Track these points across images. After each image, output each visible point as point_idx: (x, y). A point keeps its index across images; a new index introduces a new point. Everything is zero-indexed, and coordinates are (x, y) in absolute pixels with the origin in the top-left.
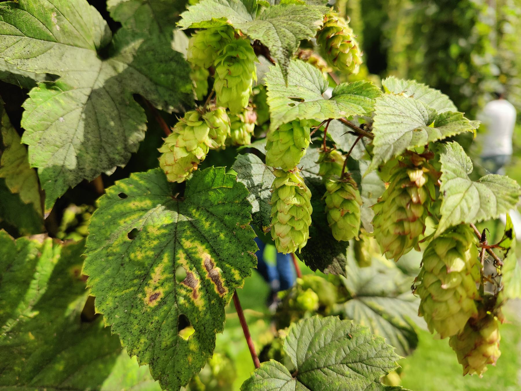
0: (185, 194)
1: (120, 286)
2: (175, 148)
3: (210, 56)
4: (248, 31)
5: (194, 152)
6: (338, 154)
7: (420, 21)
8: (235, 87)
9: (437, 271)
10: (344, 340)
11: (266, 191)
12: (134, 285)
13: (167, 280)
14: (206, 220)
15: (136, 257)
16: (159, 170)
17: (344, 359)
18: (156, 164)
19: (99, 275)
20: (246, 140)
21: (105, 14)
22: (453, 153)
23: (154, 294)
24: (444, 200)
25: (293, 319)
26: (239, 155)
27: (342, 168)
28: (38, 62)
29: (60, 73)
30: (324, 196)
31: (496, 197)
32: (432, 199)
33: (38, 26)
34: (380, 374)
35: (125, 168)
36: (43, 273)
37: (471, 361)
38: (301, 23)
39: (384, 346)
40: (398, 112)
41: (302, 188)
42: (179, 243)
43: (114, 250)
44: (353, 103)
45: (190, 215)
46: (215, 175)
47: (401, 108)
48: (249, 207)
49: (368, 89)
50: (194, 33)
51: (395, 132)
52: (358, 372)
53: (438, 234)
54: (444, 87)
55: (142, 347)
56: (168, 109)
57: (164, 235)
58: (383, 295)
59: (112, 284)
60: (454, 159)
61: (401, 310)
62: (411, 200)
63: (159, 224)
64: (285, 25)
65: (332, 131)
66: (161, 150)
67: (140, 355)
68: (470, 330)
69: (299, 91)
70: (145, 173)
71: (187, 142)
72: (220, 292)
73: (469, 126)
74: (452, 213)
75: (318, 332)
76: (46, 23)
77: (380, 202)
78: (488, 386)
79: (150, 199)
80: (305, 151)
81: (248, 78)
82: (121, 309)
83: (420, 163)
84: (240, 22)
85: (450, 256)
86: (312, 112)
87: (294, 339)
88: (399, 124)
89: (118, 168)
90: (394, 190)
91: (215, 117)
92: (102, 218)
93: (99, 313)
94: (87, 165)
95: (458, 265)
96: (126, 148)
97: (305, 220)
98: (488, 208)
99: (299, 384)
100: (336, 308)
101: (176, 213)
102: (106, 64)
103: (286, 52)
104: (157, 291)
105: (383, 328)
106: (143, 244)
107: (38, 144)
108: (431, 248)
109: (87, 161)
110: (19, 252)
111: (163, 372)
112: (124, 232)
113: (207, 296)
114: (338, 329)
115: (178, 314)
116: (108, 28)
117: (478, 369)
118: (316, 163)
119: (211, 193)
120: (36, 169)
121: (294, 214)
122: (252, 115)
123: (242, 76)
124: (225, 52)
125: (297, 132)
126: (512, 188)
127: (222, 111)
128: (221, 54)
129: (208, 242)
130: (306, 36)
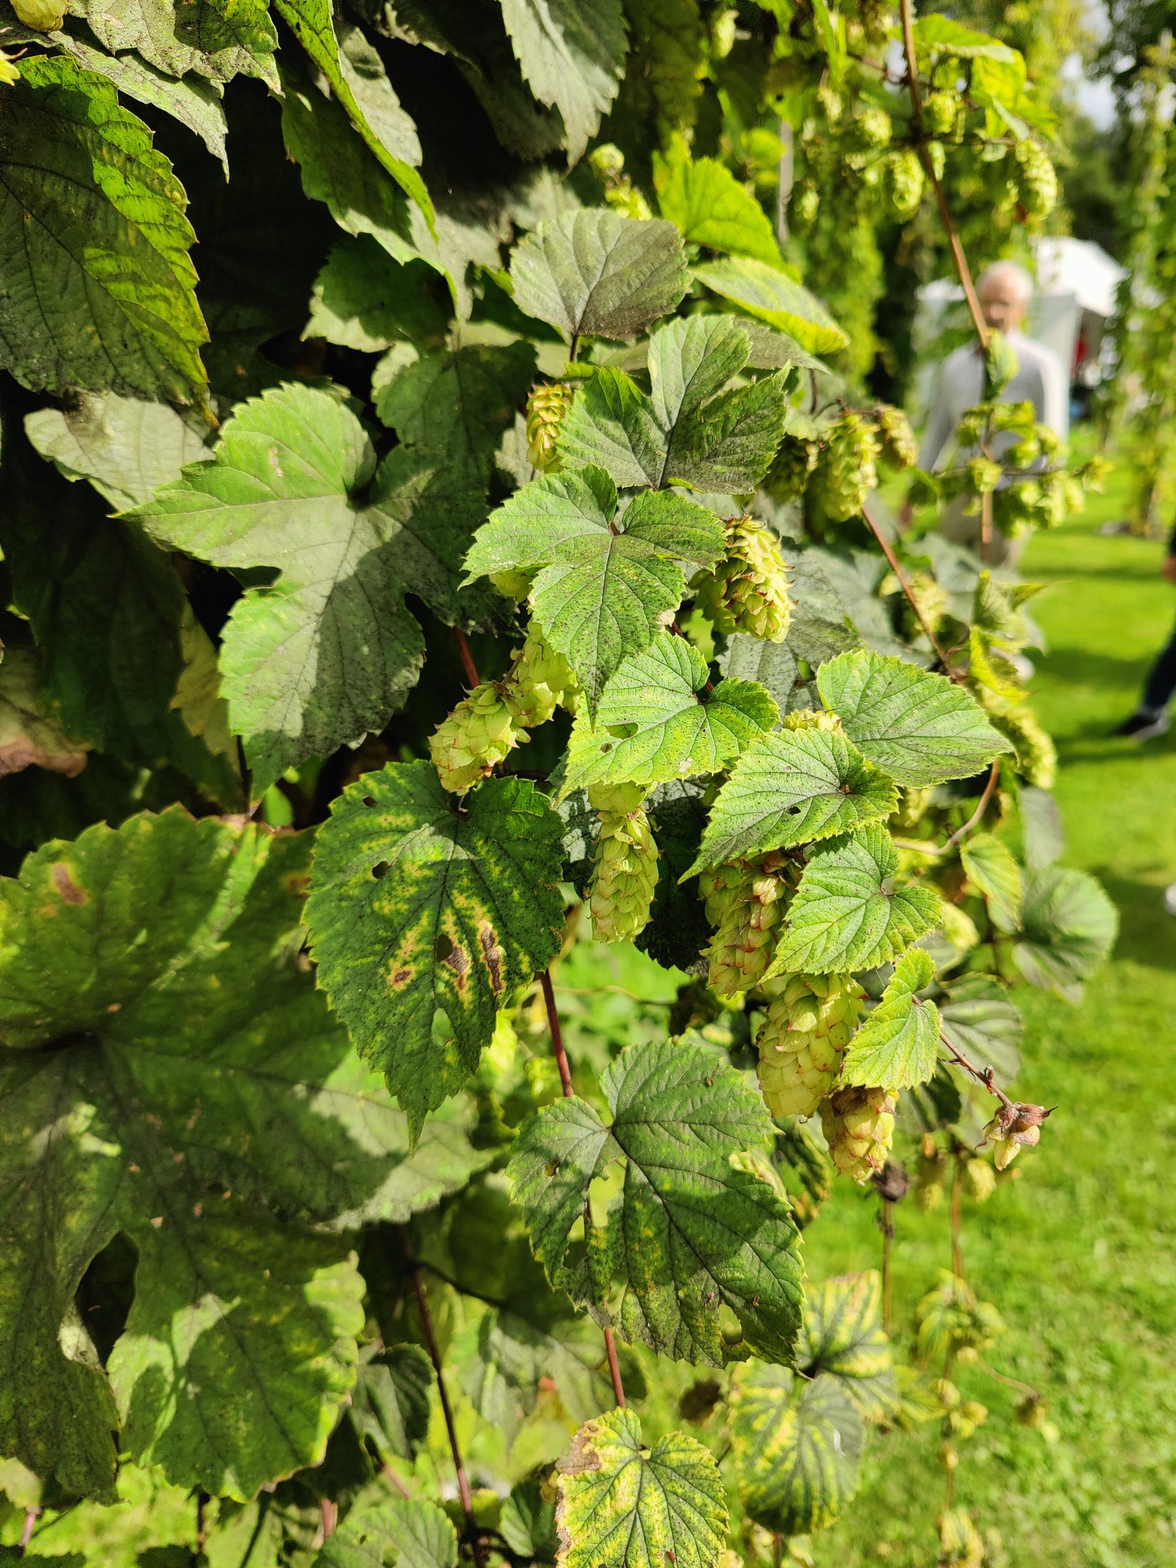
1: (354, 951)
14: (496, 864)
21: (367, 413)
25: (694, 1021)
36: (240, 879)
45: (473, 849)
46: (517, 790)
55: (376, 1047)
56: (466, 626)
57: (427, 880)
59: (343, 946)
63: (421, 859)
71: (473, 741)
79: (413, 813)
85: (801, 1005)
87: (621, 1070)
92: (336, 836)
96: (384, 699)
99: (613, 1139)
101: (452, 843)
102: (362, 516)
104: (407, 968)
110: (203, 842)
111: (404, 1086)
116: (371, 447)
119: (510, 818)
120: (239, 738)
121: (621, 887)
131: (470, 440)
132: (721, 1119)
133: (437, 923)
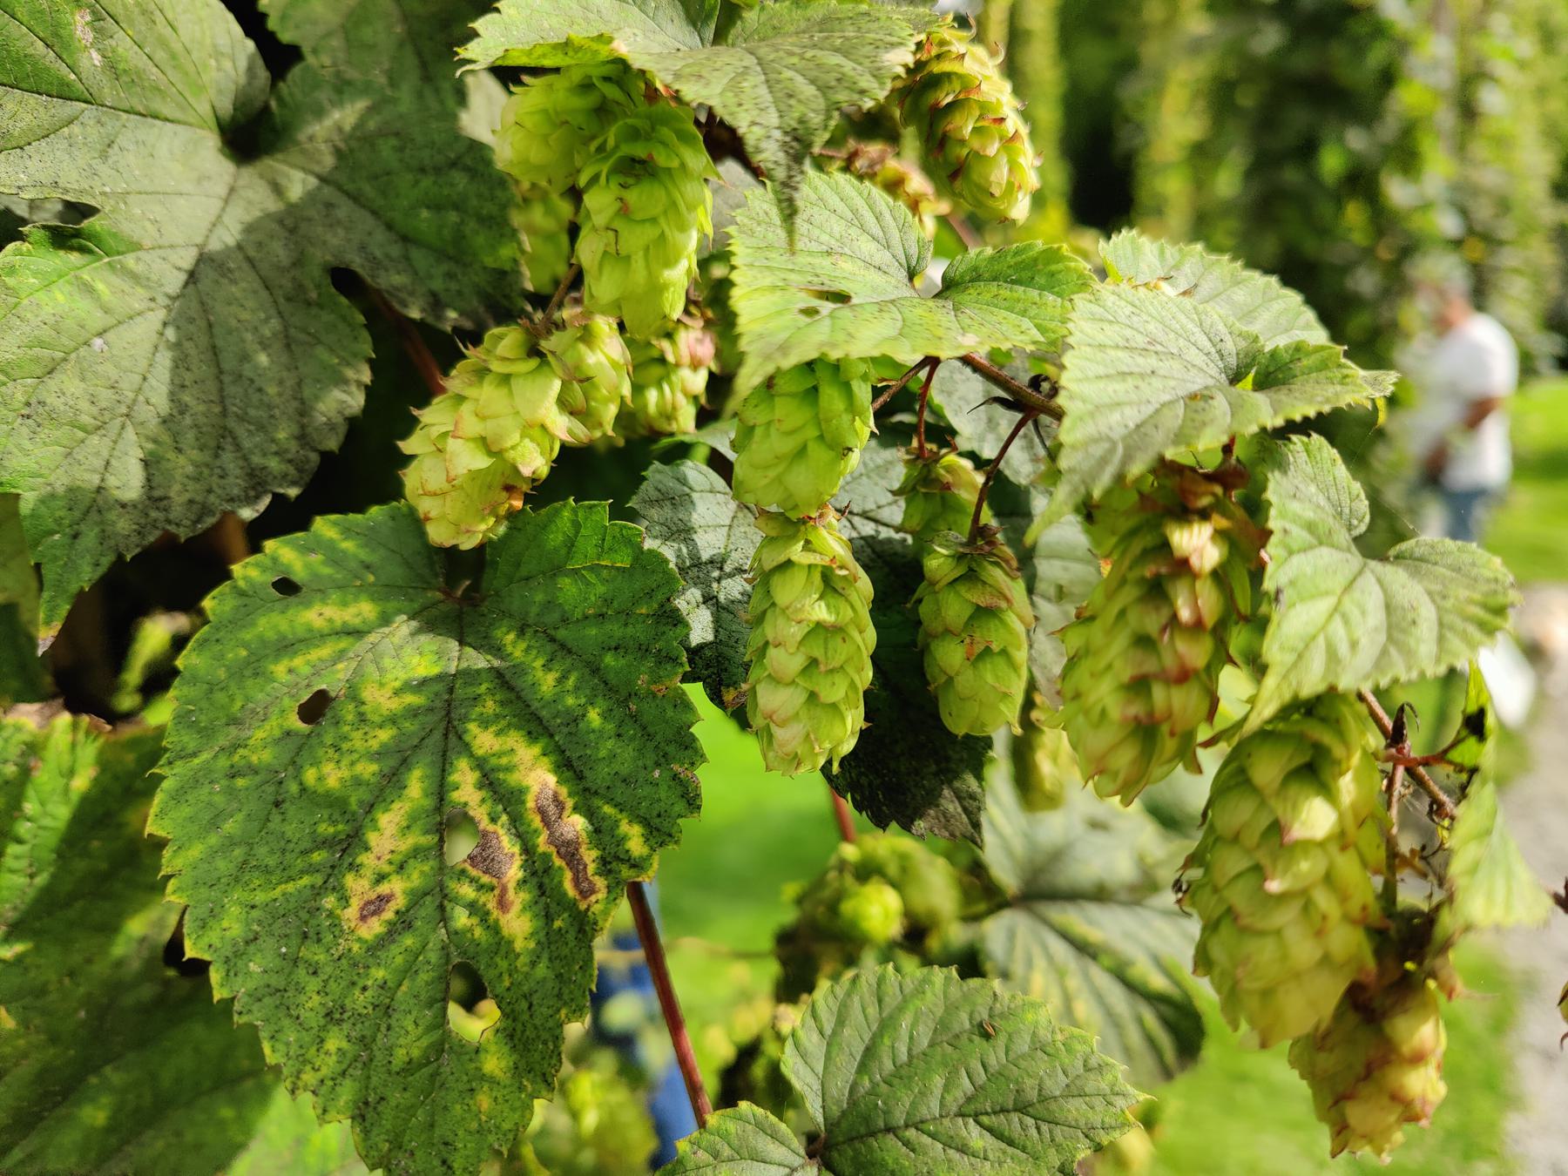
0: (484, 585)
2: (450, 441)
3: (568, 155)
4: (677, 76)
5: (511, 455)
6: (961, 467)
7: (1232, 74)
8: (641, 253)
9: (1252, 837)
10: (971, 1041)
11: (738, 578)
12: (312, 869)
13: (416, 853)
14: (547, 667)
15: (320, 779)
16: (405, 509)
17: (969, 1100)
18: (390, 490)
19: (201, 837)
20: (681, 419)
22: (1309, 469)
23: (373, 896)
24: (1275, 618)
25: (827, 967)
26: (657, 465)
27: (972, 510)
28: (29, 163)
29: (99, 198)
30: (915, 597)
31: (1439, 609)
32: (1239, 613)
33: (30, 51)
34: (1076, 1149)
35: (298, 497)
36: (47, 822)
37: (1355, 1113)
38: (846, 55)
39: (1093, 1062)
40: (1141, 341)
41: (844, 572)
42: (460, 738)
43: (254, 759)
44: (1007, 309)
45: (497, 650)
46: (577, 525)
47: (1151, 327)
48: (680, 627)
49: (1053, 267)
50: (520, 83)
51: (1130, 403)
52: (1011, 1143)
53: (1254, 723)
54: (1297, 271)
55: (329, 1065)
57: (413, 713)
58: (1100, 894)
59: (243, 866)
60: (1313, 489)
61: (1154, 943)
62: (1174, 617)
64: (795, 60)
65: (950, 394)
66: (407, 446)
67: (323, 1090)
68: (1352, 1018)
69: (836, 268)
70: (360, 516)
71: (490, 424)
72: (581, 892)
73: (1360, 388)
74: (1300, 656)
75: (891, 1017)
76: (57, 40)
77: (1084, 618)
78: (1414, 1159)
80: (855, 458)
81: (683, 228)
82: (268, 944)
83: (1205, 501)
84: (656, 49)
85: (1294, 789)
86: (876, 335)
87: (815, 1037)
88: (1142, 376)
89: (278, 499)
90: (1123, 582)
91: (582, 347)
92: (220, 657)
93: (199, 956)
94: (177, 487)
95: (1315, 818)
96: (302, 438)
97: (851, 670)
98: (1412, 642)
100: (956, 934)
101: (454, 645)
102: (248, 174)
103: (794, 144)
104: (384, 888)
105: (1099, 997)
106: (345, 738)
107: (19, 420)
108: (1234, 765)
109: (178, 474)
111: (397, 1144)
112: (287, 702)
113: (541, 905)
114: (951, 1008)
115: (447, 962)
116: (260, 62)
117: (1375, 1139)
118: (894, 493)
119: (565, 583)
121: (818, 653)
122: (700, 341)
123: (662, 221)
124: (611, 142)
125: (831, 398)
126: (1488, 581)
127: (606, 328)
128: (601, 149)
129: (551, 736)
130: (856, 97)
131: (424, 65)
132: (1033, 1095)
133: (441, 790)
